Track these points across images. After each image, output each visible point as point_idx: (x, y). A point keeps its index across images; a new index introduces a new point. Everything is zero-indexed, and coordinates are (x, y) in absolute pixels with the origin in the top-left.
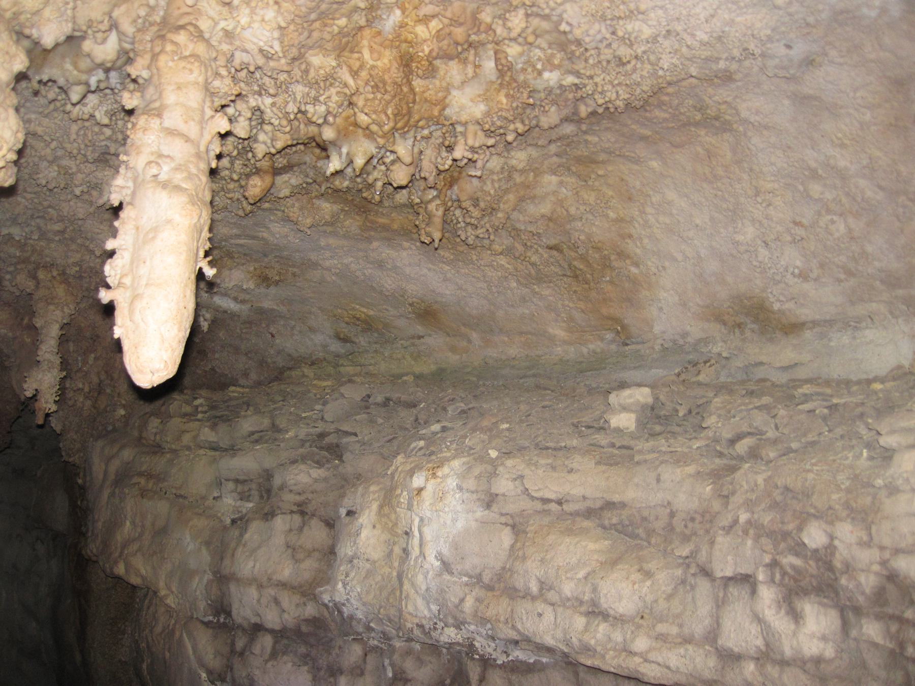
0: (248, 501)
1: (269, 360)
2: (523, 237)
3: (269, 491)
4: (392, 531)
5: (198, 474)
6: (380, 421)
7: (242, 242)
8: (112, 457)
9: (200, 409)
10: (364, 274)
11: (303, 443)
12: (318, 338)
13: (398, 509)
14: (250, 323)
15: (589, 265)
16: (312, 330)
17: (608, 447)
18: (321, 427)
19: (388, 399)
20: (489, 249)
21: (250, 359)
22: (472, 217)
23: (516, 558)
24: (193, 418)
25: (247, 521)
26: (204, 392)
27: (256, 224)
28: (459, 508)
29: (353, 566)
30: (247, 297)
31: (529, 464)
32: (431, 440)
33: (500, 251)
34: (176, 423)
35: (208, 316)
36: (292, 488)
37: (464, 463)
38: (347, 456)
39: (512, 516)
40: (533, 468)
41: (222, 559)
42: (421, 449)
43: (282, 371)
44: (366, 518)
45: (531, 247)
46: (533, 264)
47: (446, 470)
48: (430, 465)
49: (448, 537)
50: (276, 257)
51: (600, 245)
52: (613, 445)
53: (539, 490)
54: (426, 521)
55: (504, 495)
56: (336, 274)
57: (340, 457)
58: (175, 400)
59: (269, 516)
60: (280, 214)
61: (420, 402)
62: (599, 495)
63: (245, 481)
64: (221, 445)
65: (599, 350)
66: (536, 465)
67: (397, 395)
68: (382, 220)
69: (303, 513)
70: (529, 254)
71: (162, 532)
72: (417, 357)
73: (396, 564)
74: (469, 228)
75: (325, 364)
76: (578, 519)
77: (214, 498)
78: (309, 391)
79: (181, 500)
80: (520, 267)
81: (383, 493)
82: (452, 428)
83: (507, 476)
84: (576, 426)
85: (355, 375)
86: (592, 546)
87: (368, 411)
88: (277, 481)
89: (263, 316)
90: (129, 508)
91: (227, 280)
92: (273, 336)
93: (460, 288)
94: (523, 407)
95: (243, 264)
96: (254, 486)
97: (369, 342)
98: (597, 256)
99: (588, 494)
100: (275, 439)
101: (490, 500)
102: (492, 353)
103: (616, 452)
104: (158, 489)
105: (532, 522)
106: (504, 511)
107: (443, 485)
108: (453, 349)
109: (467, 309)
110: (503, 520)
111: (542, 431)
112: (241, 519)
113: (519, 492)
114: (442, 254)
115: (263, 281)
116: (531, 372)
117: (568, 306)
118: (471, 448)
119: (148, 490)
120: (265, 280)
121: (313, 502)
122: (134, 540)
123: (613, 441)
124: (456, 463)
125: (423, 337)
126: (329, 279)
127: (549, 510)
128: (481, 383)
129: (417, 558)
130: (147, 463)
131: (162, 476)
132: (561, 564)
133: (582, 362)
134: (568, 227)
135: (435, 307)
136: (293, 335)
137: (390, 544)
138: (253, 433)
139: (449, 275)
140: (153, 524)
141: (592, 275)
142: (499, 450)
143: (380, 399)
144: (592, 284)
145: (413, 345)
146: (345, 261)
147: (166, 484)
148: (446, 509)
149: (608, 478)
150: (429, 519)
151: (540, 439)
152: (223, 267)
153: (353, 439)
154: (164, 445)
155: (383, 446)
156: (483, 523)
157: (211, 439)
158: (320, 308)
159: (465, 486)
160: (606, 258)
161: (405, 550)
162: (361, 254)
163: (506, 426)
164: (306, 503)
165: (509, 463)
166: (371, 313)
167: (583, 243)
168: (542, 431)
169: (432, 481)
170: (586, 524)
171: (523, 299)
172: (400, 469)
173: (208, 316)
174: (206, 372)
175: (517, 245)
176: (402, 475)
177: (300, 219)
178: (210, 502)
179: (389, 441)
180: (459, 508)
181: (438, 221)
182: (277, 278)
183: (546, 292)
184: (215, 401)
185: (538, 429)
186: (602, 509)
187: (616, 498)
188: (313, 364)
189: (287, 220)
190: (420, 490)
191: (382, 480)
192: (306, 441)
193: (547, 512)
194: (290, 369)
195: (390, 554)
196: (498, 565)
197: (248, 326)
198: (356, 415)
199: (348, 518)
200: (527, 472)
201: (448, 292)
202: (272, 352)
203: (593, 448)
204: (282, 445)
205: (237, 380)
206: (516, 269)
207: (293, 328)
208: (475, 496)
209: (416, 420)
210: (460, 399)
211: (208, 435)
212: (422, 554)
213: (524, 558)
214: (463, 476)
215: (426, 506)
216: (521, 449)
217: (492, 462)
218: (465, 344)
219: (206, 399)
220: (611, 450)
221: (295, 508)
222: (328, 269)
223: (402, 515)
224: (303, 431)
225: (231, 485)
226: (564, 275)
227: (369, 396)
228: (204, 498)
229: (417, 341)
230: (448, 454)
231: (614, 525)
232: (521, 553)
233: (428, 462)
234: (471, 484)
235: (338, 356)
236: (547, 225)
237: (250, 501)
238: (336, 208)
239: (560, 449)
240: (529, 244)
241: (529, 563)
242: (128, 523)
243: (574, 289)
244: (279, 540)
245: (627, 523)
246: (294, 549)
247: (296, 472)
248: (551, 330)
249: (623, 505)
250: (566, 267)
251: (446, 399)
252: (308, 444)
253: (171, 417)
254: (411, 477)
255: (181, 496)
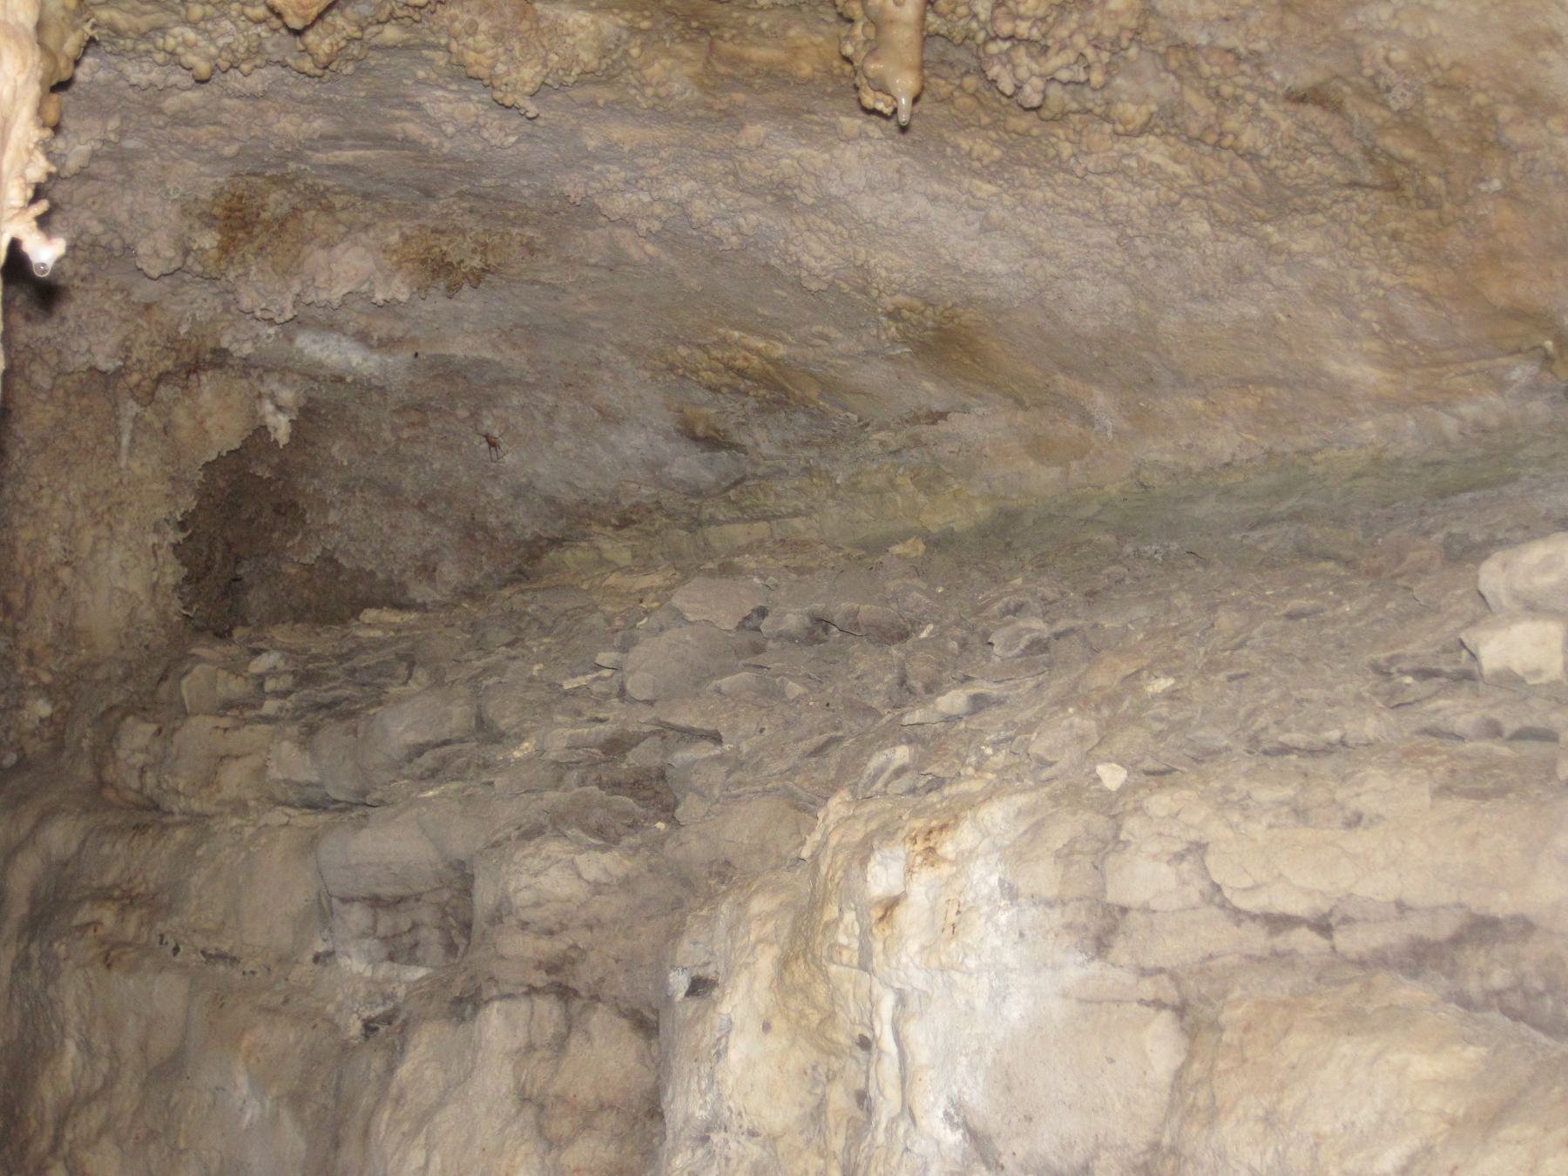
0: (413, 961)
1: (492, 520)
2: (1206, 69)
3: (467, 926)
4: (819, 1036)
5: (262, 885)
6: (795, 689)
7: (347, 156)
8: (18, 848)
9: (270, 685)
10: (738, 230)
11: (560, 768)
12: (634, 442)
13: (833, 969)
14: (420, 408)
15: (1432, 146)
16: (608, 416)
17: (1479, 737)
18: (616, 718)
19: (821, 622)
20: (1105, 118)
21: (436, 519)
22: (1017, 17)
23: (1191, 1112)
24: (249, 714)
25: (405, 1023)
26: (280, 634)
27: (377, 98)
28: (1009, 957)
29: (711, 1154)
30: (399, 329)
31: (1224, 802)
32: (927, 743)
33: (1140, 120)
34: (200, 730)
35: (287, 396)
36: (526, 915)
37: (1019, 813)
38: (690, 808)
39: (1174, 977)
40: (1236, 817)
41: (337, 1144)
42: (900, 772)
43: (535, 550)
44: (742, 1002)
45: (1237, 99)
46: (1252, 156)
47: (965, 836)
48: (918, 824)
49: (980, 1051)
50: (461, 195)
51: (1457, 73)
52: (1493, 730)
53: (1256, 887)
54: (913, 1004)
55: (1146, 909)
56: (651, 235)
57: (668, 810)
58: (199, 660)
59: (464, 1005)
60: (440, 58)
61: (917, 624)
62: (1445, 896)
63: (401, 900)
64: (334, 795)
65: (1493, 421)
66: (1243, 806)
67: (845, 605)
68: (760, 53)
69: (564, 993)
70: (1232, 123)
71: (168, 1070)
72: (931, 480)
73: (838, 1143)
74: (1021, 56)
75: (660, 520)
76: (1382, 978)
77: (316, 959)
78: (595, 608)
79: (221, 968)
80: (1214, 168)
81: (789, 918)
82: (999, 702)
83: (1154, 847)
84: (1382, 671)
85: (748, 549)
86: (1424, 1066)
87: (760, 659)
88: (485, 896)
89: (454, 388)
90: (69, 1003)
91: (321, 280)
92: (493, 444)
93: (1038, 253)
94: (1226, 620)
95: (367, 227)
96: (426, 914)
97: (785, 444)
98: (1452, 112)
99: (1414, 896)
100: (486, 766)
101: (1104, 929)
102: (1157, 451)
103: (1503, 750)
104: (155, 939)
105: (1236, 993)
106: (1150, 963)
107: (957, 886)
108: (1040, 448)
109: (1068, 317)
110: (1148, 989)
111: (1274, 694)
112: (388, 1019)
113: (1195, 898)
114: (965, 145)
115: (435, 273)
116: (1283, 507)
117: (1378, 284)
118: (1044, 763)
119: (126, 944)
120: (439, 271)
121: (593, 956)
122: (90, 1099)
123: (1497, 714)
124: (996, 814)
125: (943, 416)
126: (635, 254)
127: (1292, 952)
128: (1128, 549)
129: (893, 1120)
130: (119, 860)
131: (166, 899)
132: (1326, 1129)
133: (1441, 463)
134: (1348, 24)
135: (968, 316)
136: (553, 436)
137: (818, 1079)
138: (419, 750)
139: (996, 213)
140: (143, 1048)
141: (1444, 175)
142: (1131, 765)
143: (793, 620)
144: (1447, 207)
145: (917, 442)
146: (672, 193)
147: (176, 920)
148: (972, 963)
149: (1472, 841)
150: (925, 997)
151: (1261, 721)
152: (305, 241)
153: (706, 750)
154: (169, 802)
155: (794, 770)
156: (1090, 1002)
157: (302, 776)
158: (623, 347)
159: (1022, 884)
160: (1482, 118)
161: (862, 1097)
162: (716, 165)
163: (1163, 684)
164: (573, 962)
165: (1160, 803)
166: (780, 351)
167: (1403, 72)
168: (1274, 694)
169: (925, 876)
170: (1408, 992)
171: (1237, 274)
172: (833, 842)
173: (287, 396)
174: (309, 568)
175: (1192, 98)
176: (840, 858)
177: (501, 68)
178: (304, 970)
179: (819, 751)
180: (1009, 957)
181: (904, 36)
182: (476, 262)
183: (1304, 243)
184: (315, 658)
185: (1263, 689)
186: (1457, 941)
187: (1502, 904)
188: (625, 523)
189: (462, 75)
190: (890, 905)
191: (786, 877)
192: (570, 766)
193: (1282, 959)
194: (555, 542)
195: (818, 1113)
196: (1139, 1139)
197: (415, 417)
198: (723, 674)
199: (693, 1004)
200: (1216, 831)
201: (999, 267)
202: (498, 494)
203: (1426, 742)
204: (499, 781)
205: (403, 587)
206: (1201, 178)
207: (550, 417)
208: (1056, 917)
209: (903, 681)
210: (1036, 607)
211: (290, 761)
212: (908, 1111)
213: (1213, 1114)
214: (1017, 855)
215: (909, 955)
216: (1206, 755)
217: (1111, 807)
218: (1073, 428)
219: (289, 652)
220: (1485, 745)
221: (540, 979)
222: (626, 222)
223: (847, 986)
224: (560, 736)
225: (357, 916)
226: (1353, 184)
227: (762, 612)
228: (286, 960)
229: (926, 431)
230: (976, 786)
231: (1499, 993)
232: (1202, 1098)
233: (916, 814)
234: (1043, 876)
235: (697, 493)
236: (1281, 25)
237: (416, 962)
238: (610, 24)
239: (1328, 749)
240: (1227, 90)
241: (1226, 1128)
242: (71, 1049)
243: (1391, 225)
244: (495, 1079)
245: (1539, 985)
246: (542, 1107)
247: (536, 863)
248: (1333, 367)
249: (1525, 927)
250: (1356, 156)
251: (996, 607)
252: (574, 775)
253: (186, 714)
254: (864, 862)
255: (221, 956)
